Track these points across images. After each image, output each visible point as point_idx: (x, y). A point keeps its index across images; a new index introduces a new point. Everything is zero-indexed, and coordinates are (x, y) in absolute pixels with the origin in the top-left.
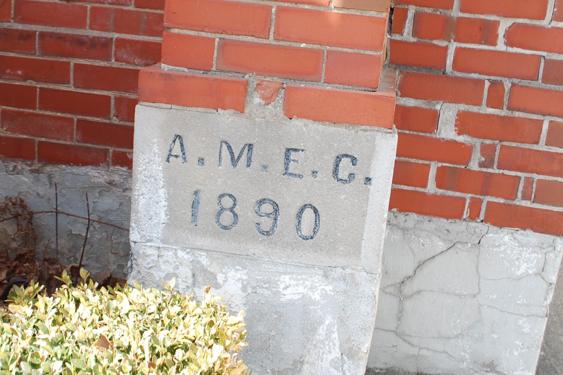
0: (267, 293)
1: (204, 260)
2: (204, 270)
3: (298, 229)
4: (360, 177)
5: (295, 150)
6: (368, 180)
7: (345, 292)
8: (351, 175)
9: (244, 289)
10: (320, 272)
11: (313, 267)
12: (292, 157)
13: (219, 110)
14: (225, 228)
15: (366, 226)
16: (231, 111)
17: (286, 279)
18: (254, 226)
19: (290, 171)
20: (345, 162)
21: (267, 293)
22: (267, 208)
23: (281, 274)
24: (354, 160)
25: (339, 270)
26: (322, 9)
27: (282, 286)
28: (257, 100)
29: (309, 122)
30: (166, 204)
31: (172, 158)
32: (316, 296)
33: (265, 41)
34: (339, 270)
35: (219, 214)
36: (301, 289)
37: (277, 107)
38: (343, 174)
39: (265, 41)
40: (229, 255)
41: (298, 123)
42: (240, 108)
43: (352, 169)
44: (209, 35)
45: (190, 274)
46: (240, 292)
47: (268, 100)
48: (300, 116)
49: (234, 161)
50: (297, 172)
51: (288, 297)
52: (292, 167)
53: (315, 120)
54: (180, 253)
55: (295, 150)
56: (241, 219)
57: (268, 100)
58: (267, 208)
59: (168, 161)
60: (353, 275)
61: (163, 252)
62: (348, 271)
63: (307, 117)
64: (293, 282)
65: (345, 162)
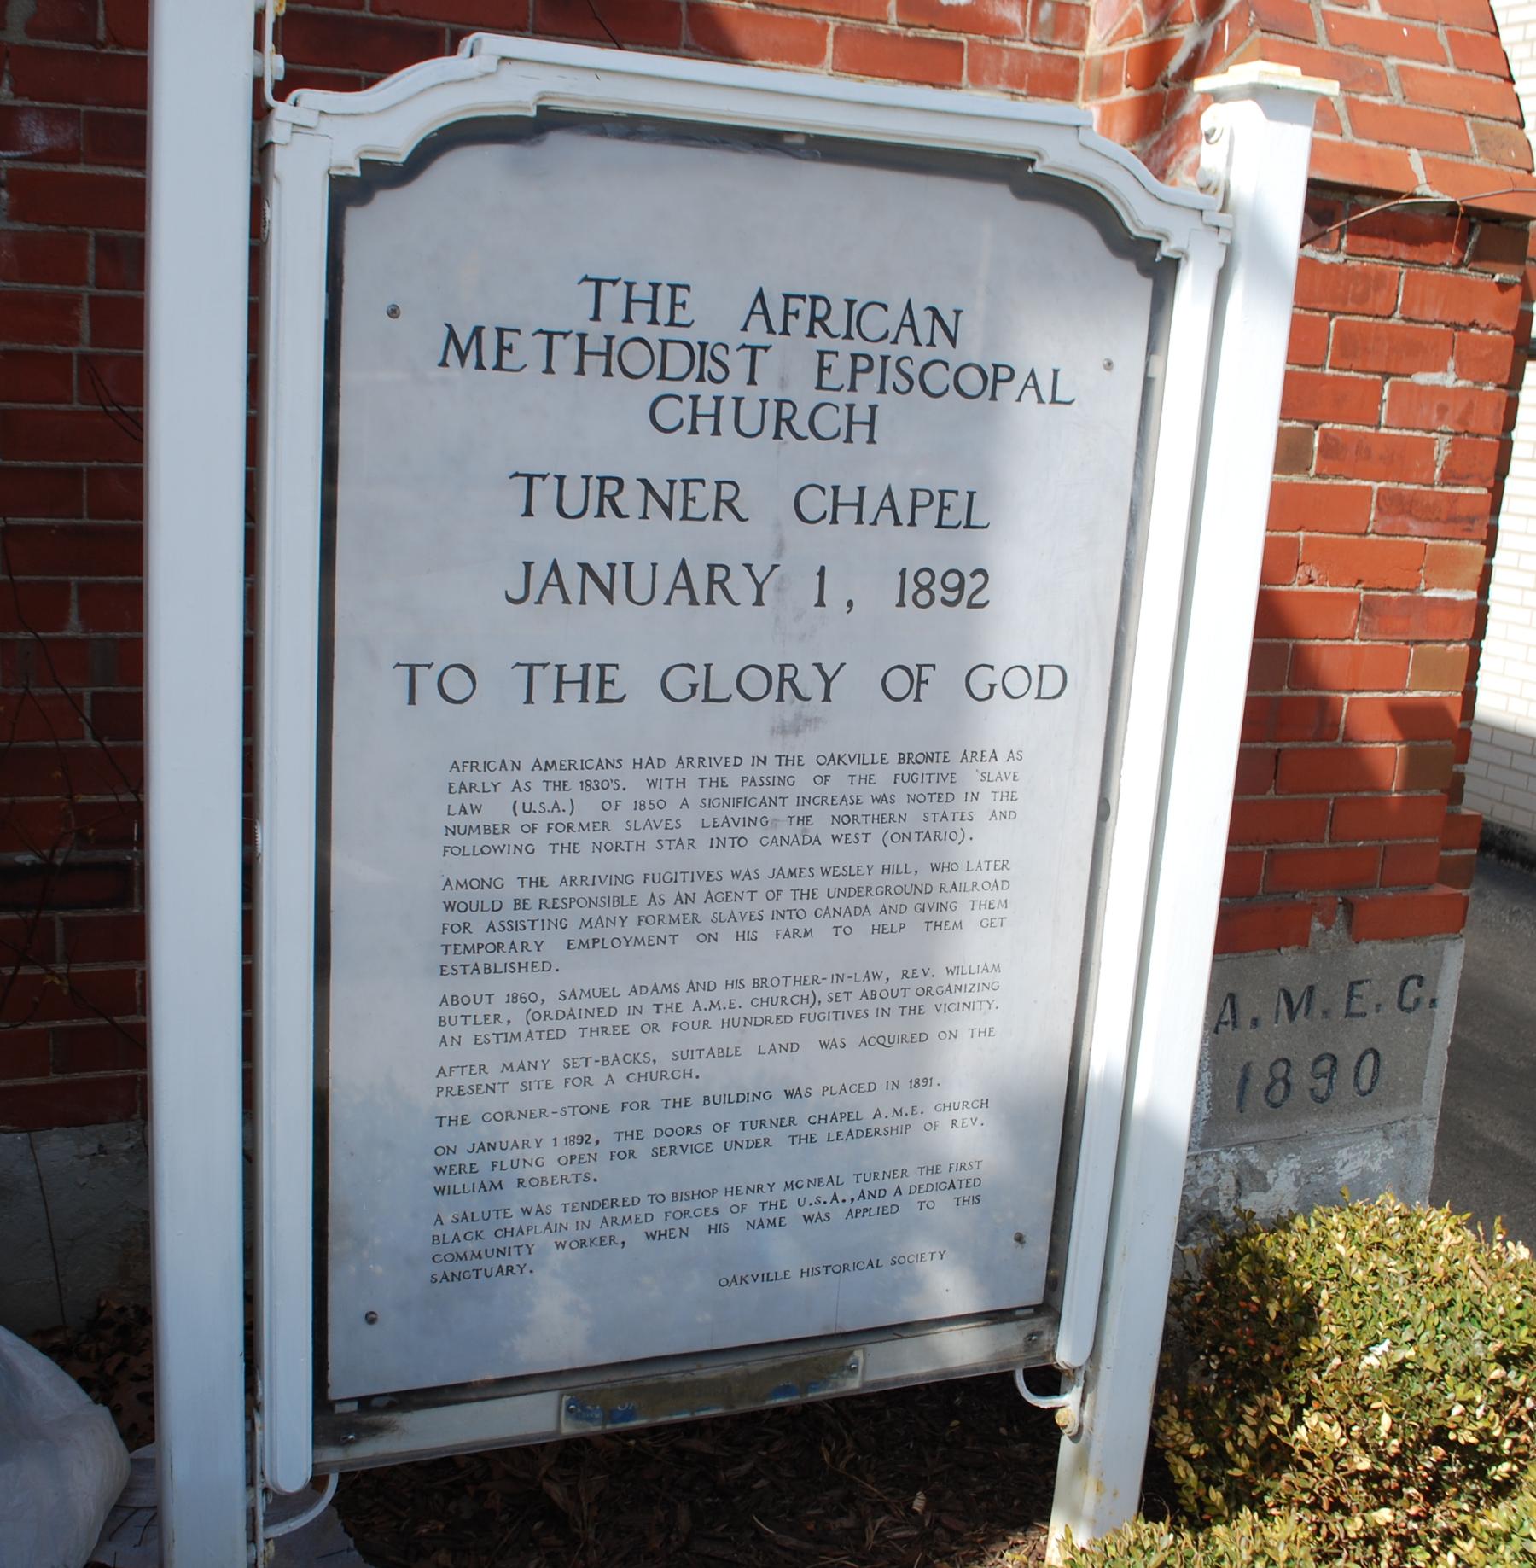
0: (1321, 1179)
1: (1253, 1157)
2: (1252, 1171)
3: (1356, 1084)
4: (1427, 1000)
5: (1360, 983)
6: (1433, 1002)
7: (1407, 1151)
8: (1417, 1001)
9: (1297, 1183)
10: (1380, 1133)
11: (1371, 1129)
12: (1355, 993)
13: (1283, 950)
14: (1275, 1106)
15: (1430, 1060)
16: (1294, 948)
17: (1343, 1154)
18: (1308, 1093)
19: (1352, 1010)
20: (1412, 983)
21: (1321, 1179)
22: (1326, 1065)
23: (1336, 1149)
24: (1420, 979)
25: (1400, 1124)
26: (1382, 795)
27: (1339, 1164)
28: (1317, 926)
29: (1377, 943)
30: (1462, 1441)
31: (1221, 1027)
32: (1376, 1167)
33: (1319, 846)
34: (1400, 1124)
35: (1269, 1089)
36: (1360, 1163)
37: (1338, 931)
38: (1409, 1001)
39: (1319, 846)
40: (1281, 1141)
41: (1365, 946)
42: (1303, 941)
43: (1419, 992)
44: (1258, 849)
45: (1233, 1182)
46: (1292, 1188)
47: (1328, 923)
48: (1368, 938)
49: (1292, 1014)
50: (1361, 1010)
51: (1345, 1178)
52: (1356, 1007)
53: (1383, 939)
54: (1224, 1156)
55: (1360, 983)
56: (1295, 1089)
57: (1328, 923)
58: (1326, 1065)
59: (1216, 1031)
60: (1414, 1126)
61: (1203, 1162)
62: (1410, 1123)
63: (1375, 938)
64: (1351, 1156)
65: (1412, 983)
